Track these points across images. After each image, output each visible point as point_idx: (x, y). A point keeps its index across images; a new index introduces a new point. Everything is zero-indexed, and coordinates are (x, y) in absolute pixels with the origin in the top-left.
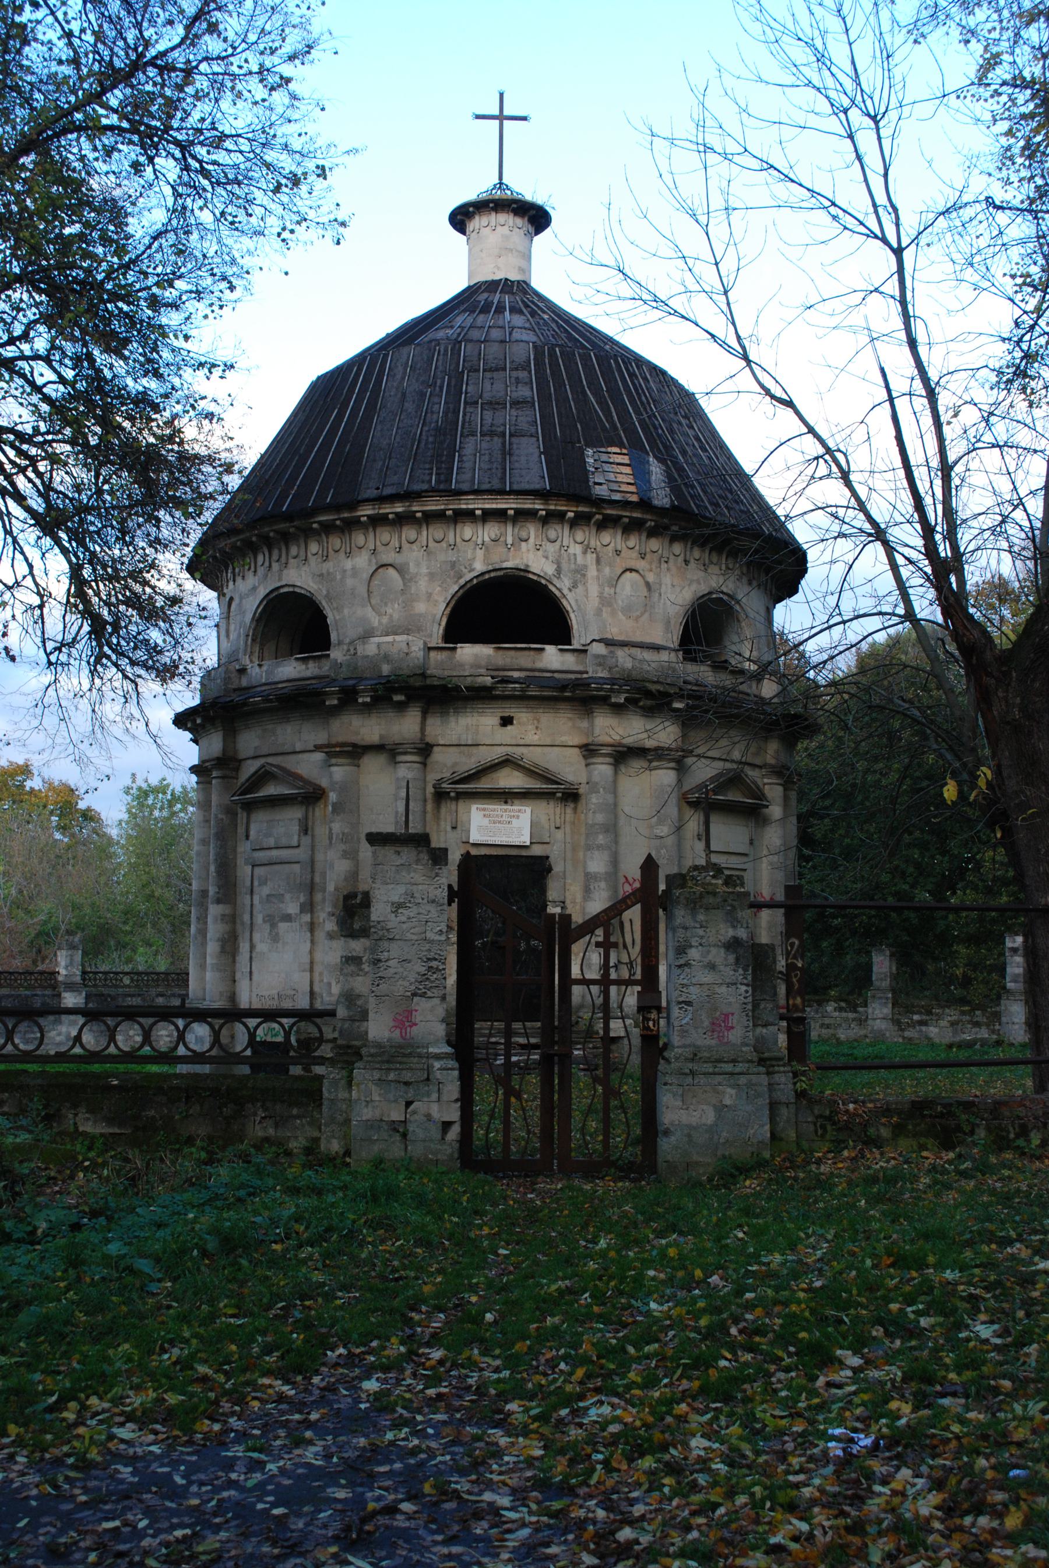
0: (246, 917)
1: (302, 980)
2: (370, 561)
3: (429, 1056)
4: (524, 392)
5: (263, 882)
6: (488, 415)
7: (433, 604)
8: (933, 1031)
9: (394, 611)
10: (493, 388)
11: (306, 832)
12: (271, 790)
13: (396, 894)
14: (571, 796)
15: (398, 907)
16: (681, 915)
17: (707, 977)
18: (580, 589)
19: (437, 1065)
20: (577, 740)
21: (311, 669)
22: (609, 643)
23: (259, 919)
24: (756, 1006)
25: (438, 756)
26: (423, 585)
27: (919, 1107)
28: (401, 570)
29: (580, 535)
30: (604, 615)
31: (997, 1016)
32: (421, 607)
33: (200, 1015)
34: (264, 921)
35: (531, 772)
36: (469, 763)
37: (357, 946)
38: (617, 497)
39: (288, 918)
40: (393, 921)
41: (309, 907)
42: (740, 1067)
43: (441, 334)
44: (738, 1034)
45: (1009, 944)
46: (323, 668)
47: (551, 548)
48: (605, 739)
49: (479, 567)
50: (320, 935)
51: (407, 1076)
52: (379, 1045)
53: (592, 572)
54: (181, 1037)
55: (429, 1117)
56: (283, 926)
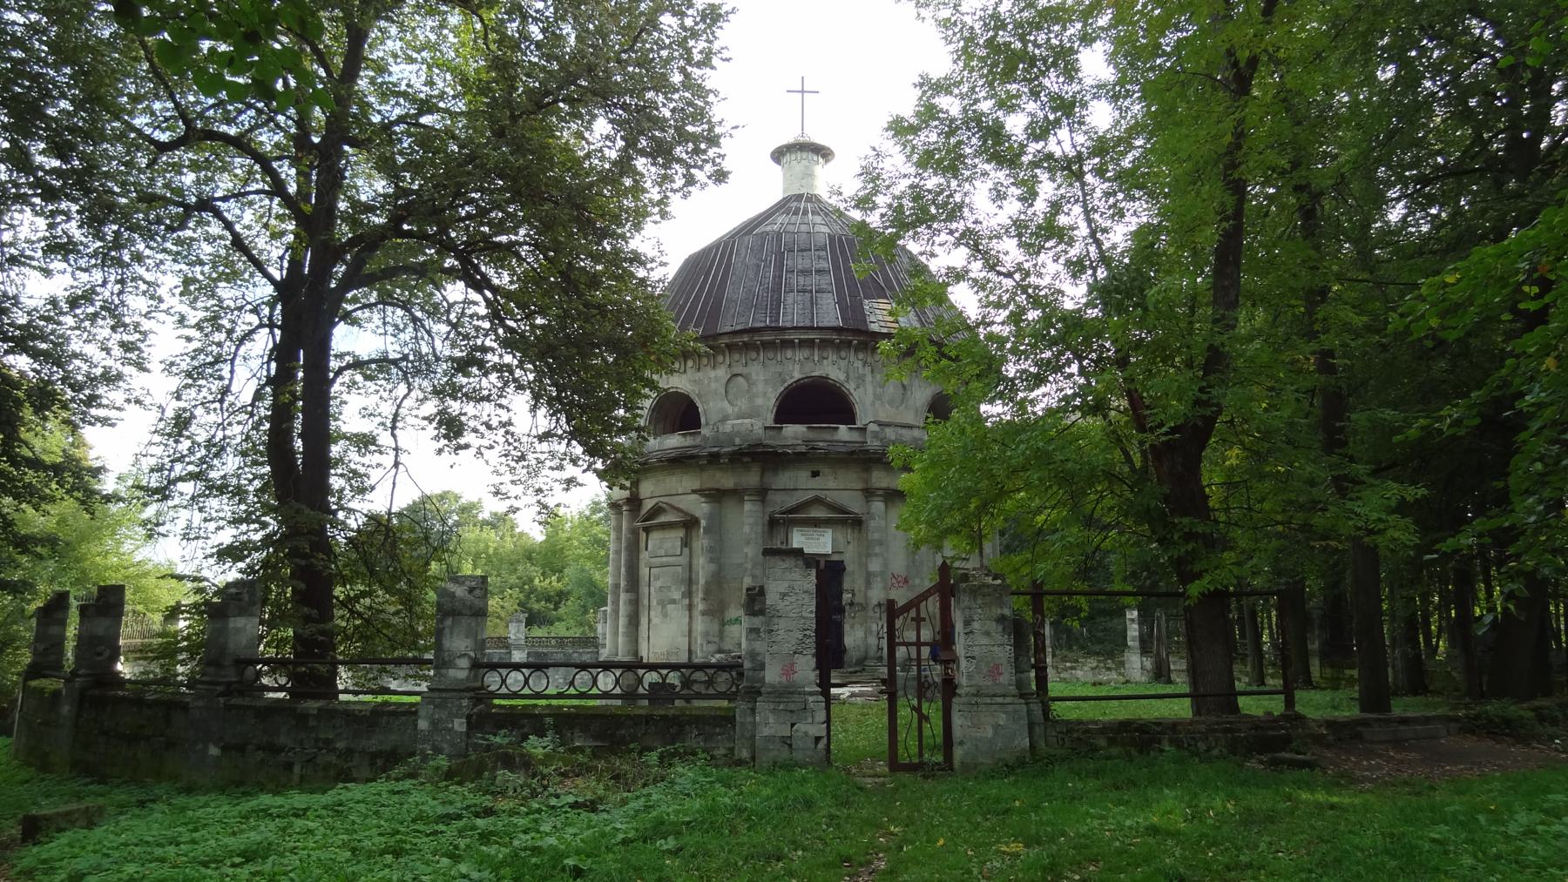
0: (646, 602)
1: (683, 643)
3: (805, 693)
4: (824, 265)
5: (657, 578)
6: (801, 279)
7: (767, 399)
8: (1079, 673)
9: (743, 404)
10: (801, 262)
12: (663, 519)
13: (783, 587)
14: (857, 523)
15: (784, 595)
16: (966, 600)
17: (985, 641)
18: (861, 389)
19: (811, 699)
20: (860, 486)
21: (689, 441)
22: (880, 424)
23: (654, 602)
24: (1016, 659)
25: (770, 496)
26: (761, 387)
27: (1125, 725)
28: (747, 377)
29: (861, 356)
31: (1122, 664)
32: (759, 401)
33: (607, 666)
35: (832, 507)
36: (792, 501)
37: (757, 621)
38: (885, 331)
39: (673, 602)
40: (781, 605)
41: (689, 594)
42: (1008, 700)
43: (769, 228)
44: (1007, 677)
45: (1128, 616)
46: (698, 440)
47: (843, 363)
48: (877, 485)
49: (797, 375)
51: (792, 707)
52: (773, 686)
53: (869, 378)
54: (504, 681)
55: (806, 734)
56: (670, 607)
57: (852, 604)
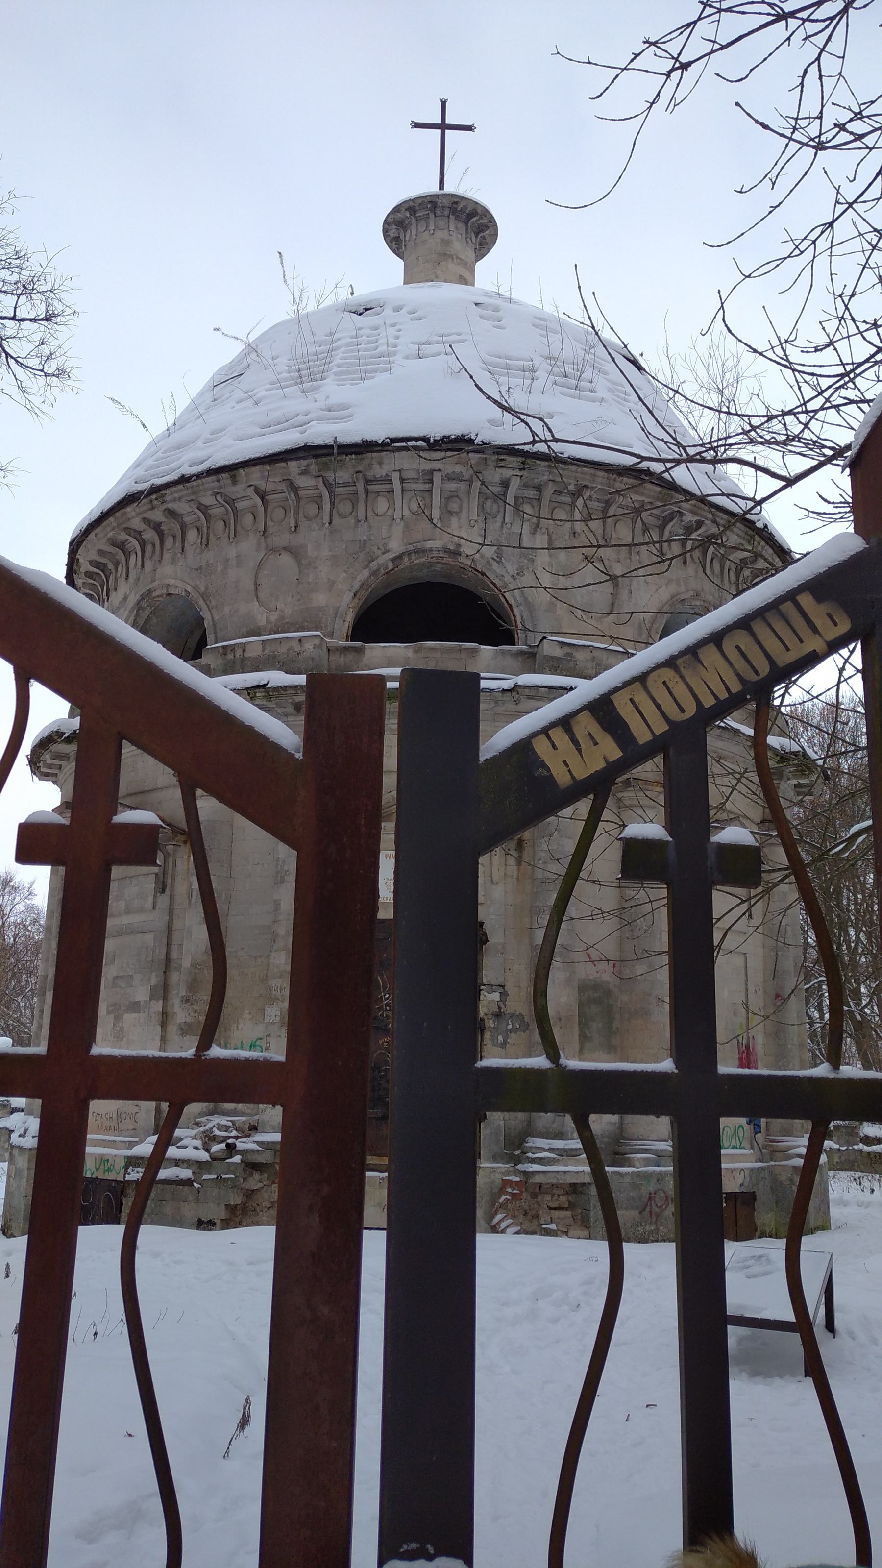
2: (259, 545)
7: (338, 595)
11: (163, 891)
26: (324, 571)
30: (559, 611)
32: (320, 599)
34: (108, 1012)
39: (135, 1007)
41: (163, 991)
49: (396, 546)
50: (173, 1029)
56: (129, 1018)
57: (498, 1015)
